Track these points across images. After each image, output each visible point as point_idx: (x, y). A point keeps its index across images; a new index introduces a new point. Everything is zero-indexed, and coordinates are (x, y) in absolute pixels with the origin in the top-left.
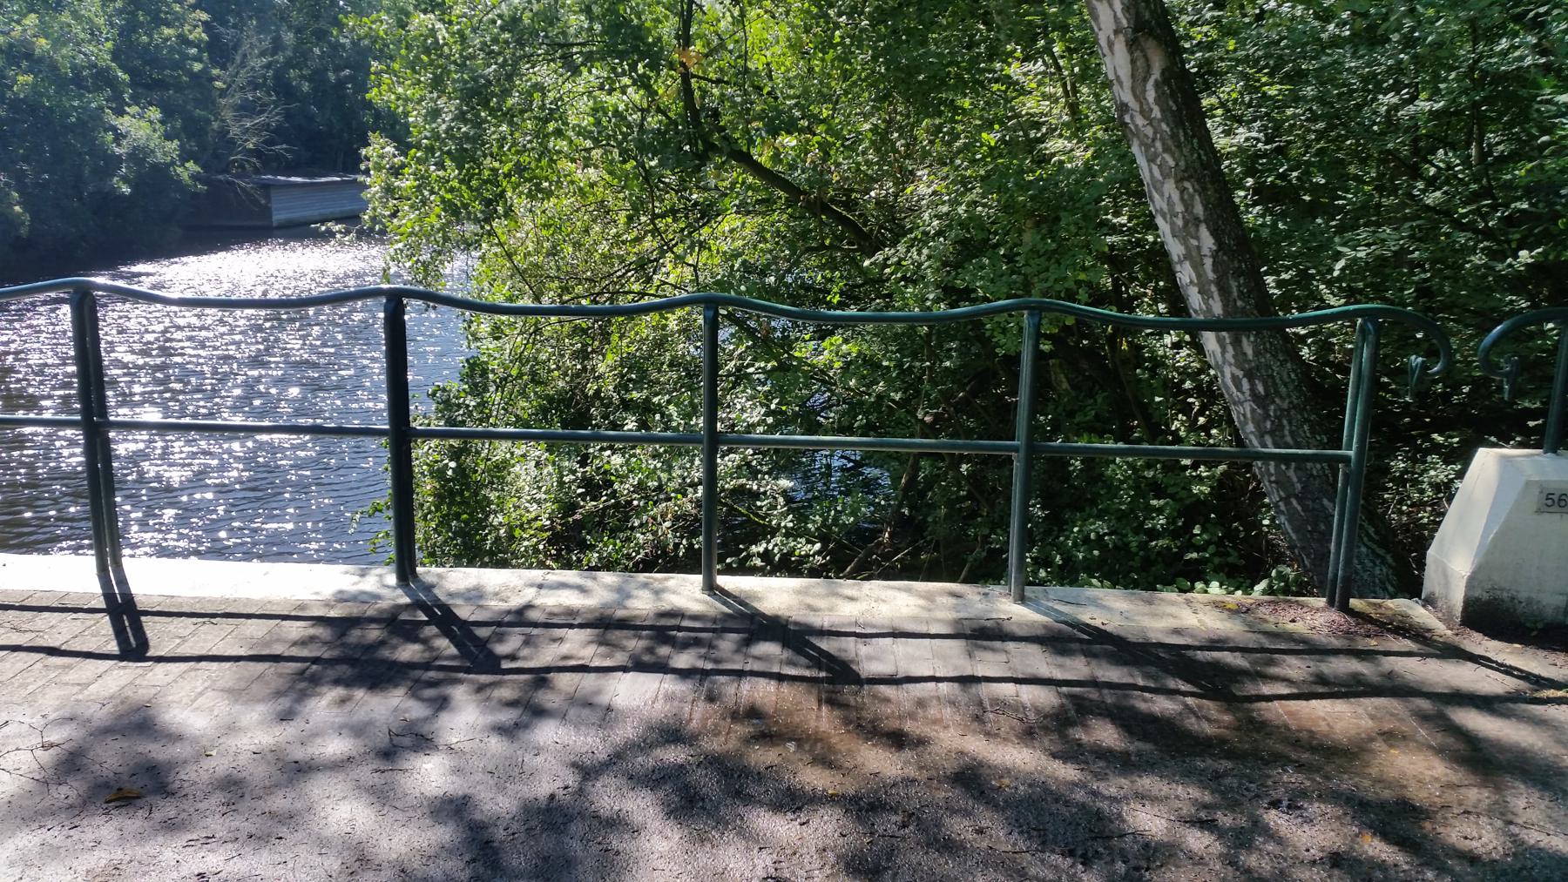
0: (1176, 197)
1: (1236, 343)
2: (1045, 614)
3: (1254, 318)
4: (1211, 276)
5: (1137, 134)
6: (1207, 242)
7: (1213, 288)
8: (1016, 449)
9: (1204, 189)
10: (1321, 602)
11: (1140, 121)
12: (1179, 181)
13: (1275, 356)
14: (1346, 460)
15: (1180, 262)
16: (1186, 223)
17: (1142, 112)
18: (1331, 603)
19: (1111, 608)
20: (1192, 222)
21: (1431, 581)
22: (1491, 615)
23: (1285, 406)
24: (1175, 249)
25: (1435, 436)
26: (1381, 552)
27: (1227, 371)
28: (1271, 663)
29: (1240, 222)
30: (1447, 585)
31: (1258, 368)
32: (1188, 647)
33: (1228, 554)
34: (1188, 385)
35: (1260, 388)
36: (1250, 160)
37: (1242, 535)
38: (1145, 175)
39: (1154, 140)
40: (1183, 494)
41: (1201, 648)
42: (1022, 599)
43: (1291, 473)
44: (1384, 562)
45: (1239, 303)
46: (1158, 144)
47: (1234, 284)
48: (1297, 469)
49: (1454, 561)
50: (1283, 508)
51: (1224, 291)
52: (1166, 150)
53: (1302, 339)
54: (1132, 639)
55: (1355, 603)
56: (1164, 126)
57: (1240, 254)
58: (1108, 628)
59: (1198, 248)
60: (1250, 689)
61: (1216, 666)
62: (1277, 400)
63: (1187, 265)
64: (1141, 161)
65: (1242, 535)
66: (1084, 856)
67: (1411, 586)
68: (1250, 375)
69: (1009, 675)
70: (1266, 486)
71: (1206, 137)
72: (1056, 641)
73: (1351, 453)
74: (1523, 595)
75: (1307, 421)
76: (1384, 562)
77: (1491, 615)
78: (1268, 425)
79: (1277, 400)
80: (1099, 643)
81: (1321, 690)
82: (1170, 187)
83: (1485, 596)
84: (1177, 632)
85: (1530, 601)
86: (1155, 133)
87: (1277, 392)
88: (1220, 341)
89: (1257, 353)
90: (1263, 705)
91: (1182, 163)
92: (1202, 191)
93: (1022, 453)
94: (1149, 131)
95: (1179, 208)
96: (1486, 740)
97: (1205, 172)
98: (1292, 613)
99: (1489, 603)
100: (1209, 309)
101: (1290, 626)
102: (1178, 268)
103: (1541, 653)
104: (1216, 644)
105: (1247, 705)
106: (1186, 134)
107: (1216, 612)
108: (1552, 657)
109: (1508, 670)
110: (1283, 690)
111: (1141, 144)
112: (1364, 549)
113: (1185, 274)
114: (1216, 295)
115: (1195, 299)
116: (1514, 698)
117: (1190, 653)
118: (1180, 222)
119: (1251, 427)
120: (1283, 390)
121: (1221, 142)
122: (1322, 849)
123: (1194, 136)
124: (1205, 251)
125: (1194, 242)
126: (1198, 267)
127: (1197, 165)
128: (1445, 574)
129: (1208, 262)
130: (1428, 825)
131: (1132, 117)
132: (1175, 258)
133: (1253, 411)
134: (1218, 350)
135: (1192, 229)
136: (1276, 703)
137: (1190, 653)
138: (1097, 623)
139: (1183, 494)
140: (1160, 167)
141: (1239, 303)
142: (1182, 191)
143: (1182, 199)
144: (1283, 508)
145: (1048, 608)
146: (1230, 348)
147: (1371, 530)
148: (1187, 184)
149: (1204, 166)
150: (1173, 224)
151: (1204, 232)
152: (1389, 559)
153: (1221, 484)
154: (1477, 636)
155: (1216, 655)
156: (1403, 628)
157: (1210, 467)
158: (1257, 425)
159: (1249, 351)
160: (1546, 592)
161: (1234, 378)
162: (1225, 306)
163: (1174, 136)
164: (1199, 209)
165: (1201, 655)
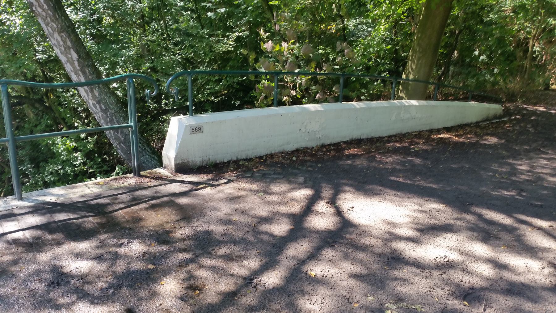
0: (59, 39)
1: (92, 91)
2: (32, 202)
3: (95, 81)
4: (78, 68)
5: (39, 14)
6: (75, 56)
7: (80, 72)
8: (7, 141)
9: (70, 36)
10: (132, 175)
11: (40, 10)
12: (59, 33)
13: (106, 95)
14: (131, 127)
15: (66, 63)
16: (65, 49)
17: (39, 6)
18: (135, 175)
19: (57, 194)
20: (67, 48)
21: (165, 161)
22: (183, 168)
23: (113, 112)
24: (63, 59)
25: (164, 116)
26: (153, 156)
27: (91, 102)
28: (116, 199)
29: (85, 48)
30: (169, 161)
31: (101, 99)
32: (88, 200)
33: (103, 167)
34: (79, 109)
35: (103, 107)
36: (85, 23)
37: (108, 159)
38: (46, 32)
39: (46, 17)
40: (85, 149)
41: (92, 200)
42: (21, 199)
43: (119, 135)
44: (154, 158)
45: (90, 77)
46: (49, 19)
47: (87, 71)
48: (122, 133)
49: (170, 153)
50: (118, 147)
51: (84, 73)
52: (52, 21)
53: (117, 89)
54: (67, 203)
55: (142, 173)
56: (50, 12)
57: (86, 58)
58: (58, 202)
59: (72, 58)
60: (110, 209)
61: (98, 204)
62: (110, 111)
63: (68, 64)
64: (43, 25)
65: (108, 159)
66: (58, 283)
67: (160, 163)
68: (99, 102)
69: (20, 228)
70: (112, 141)
71: (67, 17)
72: (37, 209)
73: (132, 124)
74: (190, 160)
75: (121, 116)
76: (154, 158)
77: (183, 168)
78: (108, 119)
79: (110, 111)
80: (55, 207)
81: (134, 203)
82: (56, 35)
83: (181, 162)
84: (83, 196)
85: (193, 161)
86: (46, 15)
87: (109, 107)
88: (86, 91)
89: (100, 95)
90: (116, 213)
91: (59, 26)
92: (69, 36)
93: (10, 142)
94: (44, 14)
95: (62, 43)
96: (183, 205)
97: (69, 28)
98: (123, 181)
99: (182, 164)
100: (80, 80)
101: (122, 185)
102: (65, 66)
103: (197, 176)
104: (98, 197)
105: (110, 215)
106: (59, 15)
107: (96, 186)
108: (200, 176)
109: (189, 183)
110: (122, 206)
111: (42, 19)
112: (147, 156)
113: (68, 68)
114: (81, 75)
115: (74, 78)
116: (191, 190)
117: (89, 202)
118: (63, 49)
119: (102, 121)
120: (111, 107)
121: (73, 17)
122: (140, 253)
123: (62, 16)
124: (74, 59)
125: (70, 56)
126: (72, 64)
127: (65, 26)
128: (169, 159)
129: (76, 63)
130: (171, 235)
131: (36, 8)
132: (64, 62)
133: (102, 115)
134: (86, 95)
135: (68, 51)
136: (120, 211)
137: (89, 202)
138: (53, 200)
139: (85, 149)
140: (51, 27)
141: (90, 77)
142: (62, 37)
143: (62, 40)
144: (118, 147)
145: (33, 200)
146: (90, 94)
147: (149, 150)
148: (63, 34)
149: (69, 27)
150: (60, 50)
151: (73, 52)
152: (156, 158)
153: (97, 142)
154: (180, 175)
155: (98, 201)
156: (157, 178)
157: (92, 137)
158: (105, 121)
159: (97, 94)
160: (196, 158)
161: (93, 104)
162: (85, 79)
163: (54, 16)
164: (69, 43)
165: (93, 202)
